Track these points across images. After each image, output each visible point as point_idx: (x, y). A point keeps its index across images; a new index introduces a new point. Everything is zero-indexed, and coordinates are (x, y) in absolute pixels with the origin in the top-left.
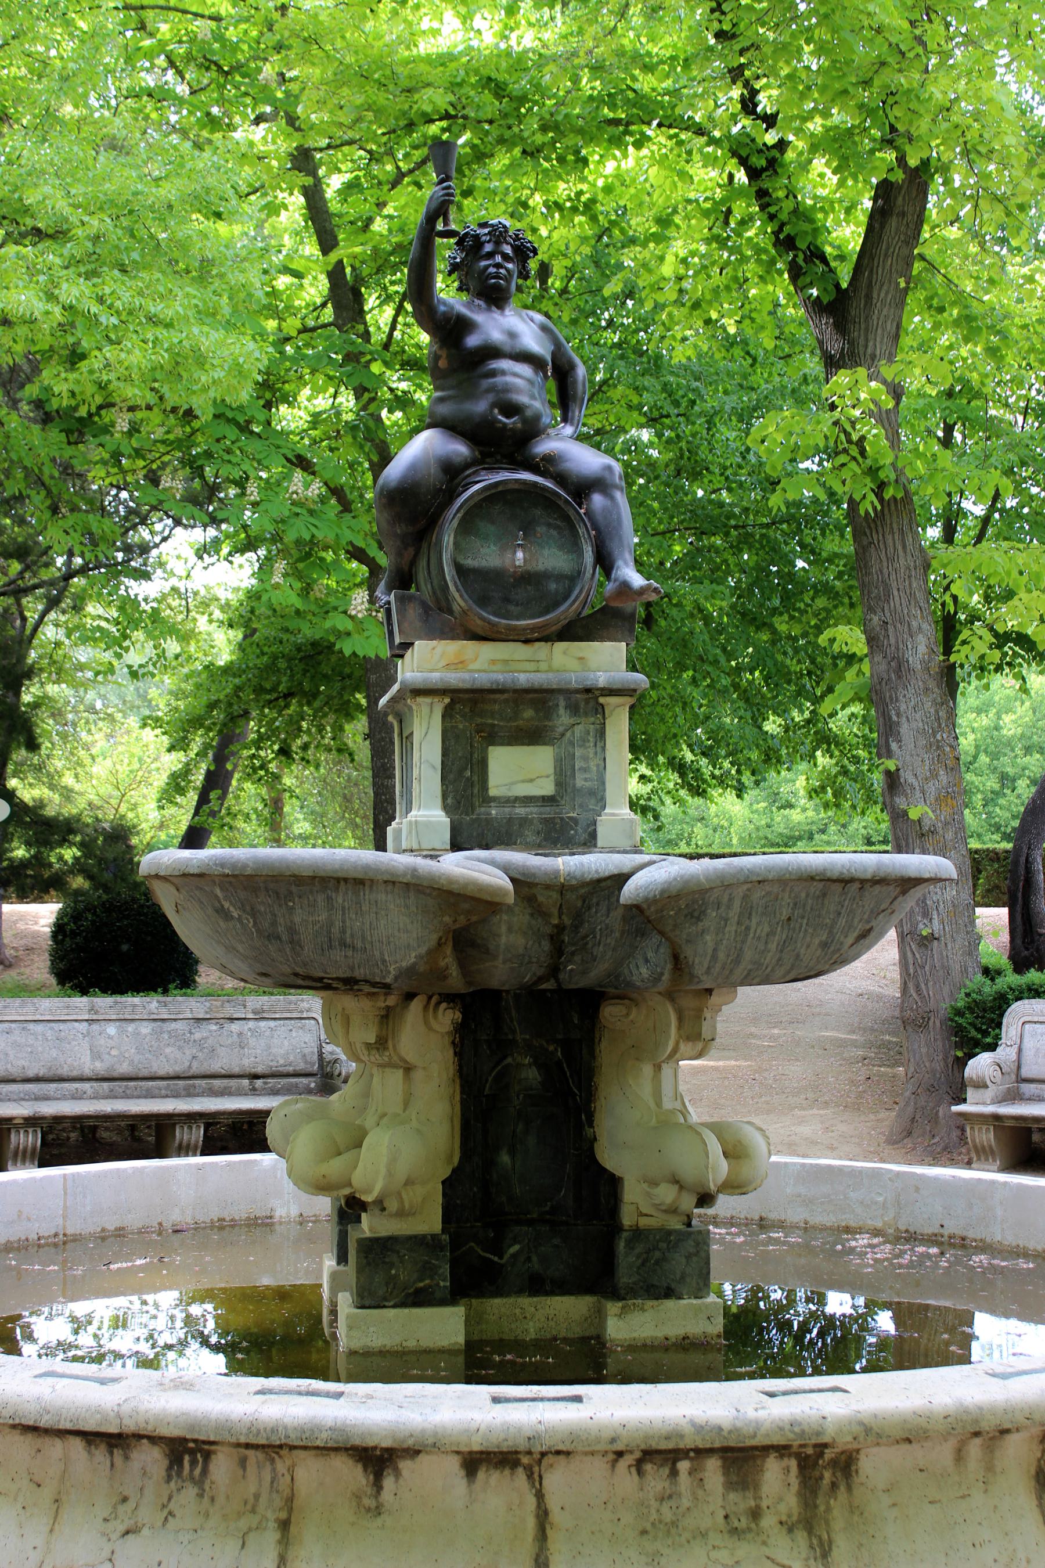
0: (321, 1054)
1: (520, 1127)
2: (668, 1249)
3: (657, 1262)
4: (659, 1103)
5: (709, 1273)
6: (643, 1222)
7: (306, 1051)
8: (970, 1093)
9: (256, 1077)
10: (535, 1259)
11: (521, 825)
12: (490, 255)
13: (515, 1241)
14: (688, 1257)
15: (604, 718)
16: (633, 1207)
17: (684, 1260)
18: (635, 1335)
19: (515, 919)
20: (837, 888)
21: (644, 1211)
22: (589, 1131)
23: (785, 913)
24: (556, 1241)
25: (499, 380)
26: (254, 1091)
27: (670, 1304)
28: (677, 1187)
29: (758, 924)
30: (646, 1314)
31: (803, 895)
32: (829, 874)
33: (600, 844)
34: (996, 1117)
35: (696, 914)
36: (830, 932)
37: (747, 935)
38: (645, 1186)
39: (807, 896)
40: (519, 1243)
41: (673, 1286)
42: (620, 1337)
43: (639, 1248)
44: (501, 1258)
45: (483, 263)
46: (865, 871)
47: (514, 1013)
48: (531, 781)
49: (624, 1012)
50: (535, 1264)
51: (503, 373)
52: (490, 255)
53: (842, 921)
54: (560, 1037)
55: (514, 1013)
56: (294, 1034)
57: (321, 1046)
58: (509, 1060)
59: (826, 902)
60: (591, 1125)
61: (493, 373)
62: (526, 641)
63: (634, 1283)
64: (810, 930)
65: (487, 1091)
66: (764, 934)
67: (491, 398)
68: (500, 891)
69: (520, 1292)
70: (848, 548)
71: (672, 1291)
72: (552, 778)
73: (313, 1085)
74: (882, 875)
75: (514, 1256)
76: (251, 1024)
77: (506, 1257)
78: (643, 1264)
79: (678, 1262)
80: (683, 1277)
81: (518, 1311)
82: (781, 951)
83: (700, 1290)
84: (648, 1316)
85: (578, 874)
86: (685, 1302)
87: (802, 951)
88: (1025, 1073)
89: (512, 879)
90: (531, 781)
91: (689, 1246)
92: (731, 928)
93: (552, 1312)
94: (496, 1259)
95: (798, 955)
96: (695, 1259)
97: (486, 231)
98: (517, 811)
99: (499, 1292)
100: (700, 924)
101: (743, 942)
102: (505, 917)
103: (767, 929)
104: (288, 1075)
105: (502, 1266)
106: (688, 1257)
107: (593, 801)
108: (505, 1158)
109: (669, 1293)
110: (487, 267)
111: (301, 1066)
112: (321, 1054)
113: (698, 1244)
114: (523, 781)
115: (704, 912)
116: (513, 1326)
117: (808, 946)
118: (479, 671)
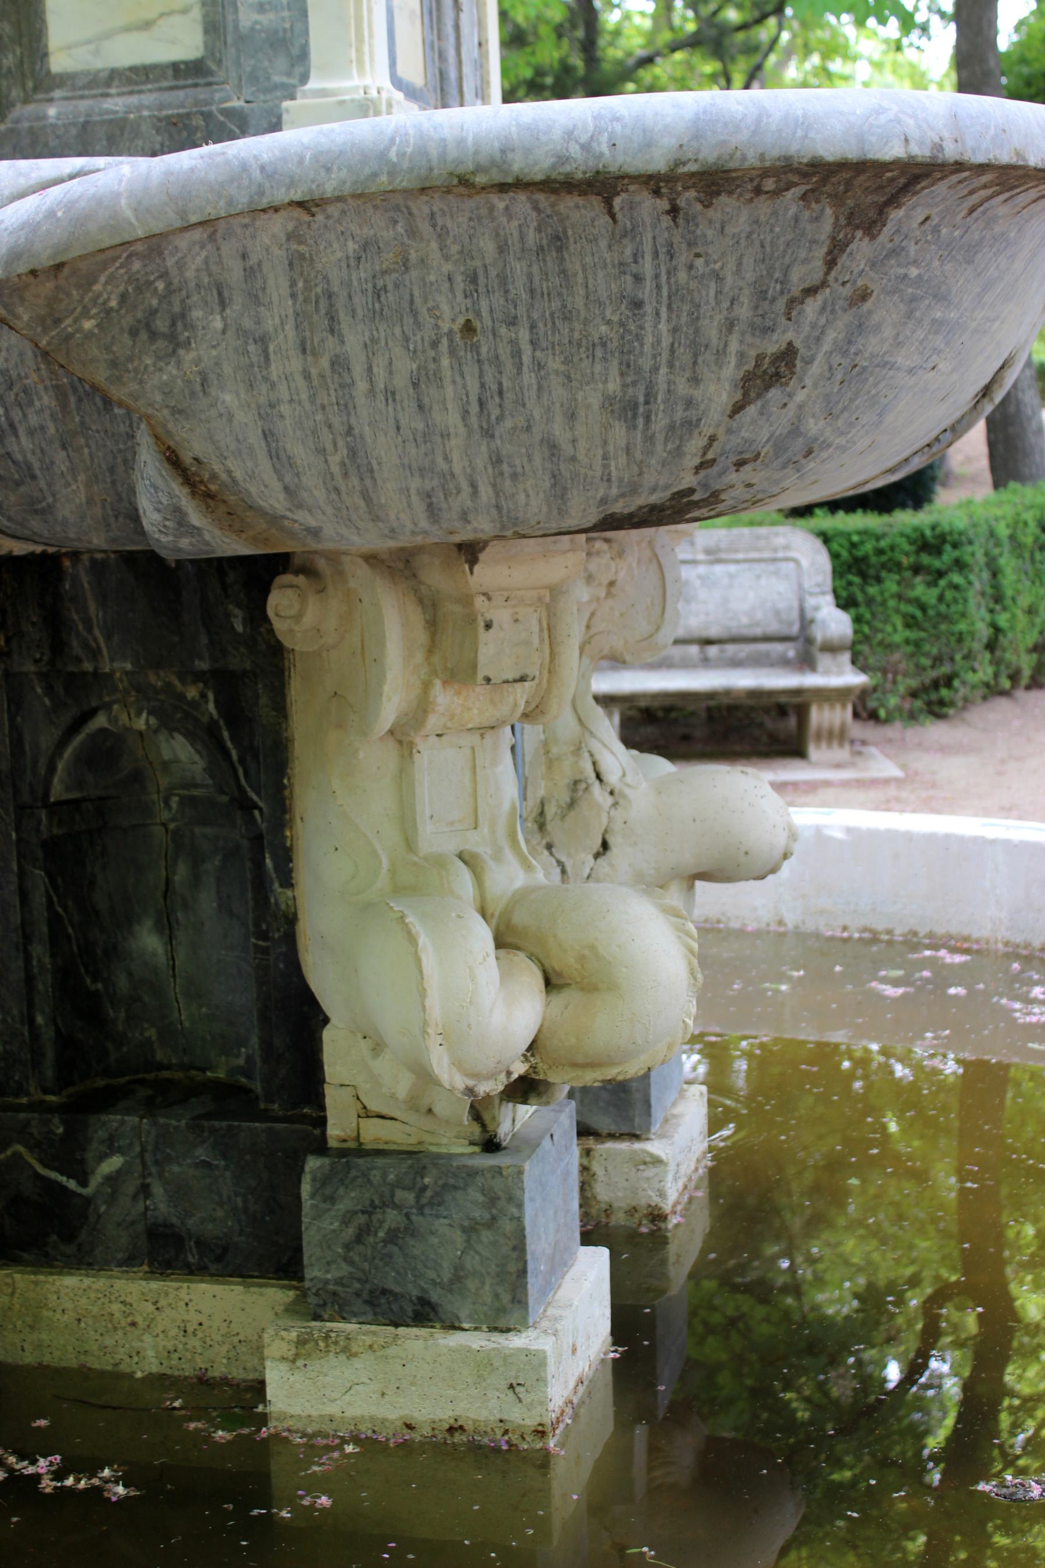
1: (182, 872)
2: (421, 1209)
3: (393, 1237)
5: (523, 1272)
6: (373, 1132)
7: (782, 605)
9: (708, 642)
10: (158, 1190)
13: (112, 1147)
14: (471, 1230)
16: (346, 1094)
17: (459, 1237)
18: (333, 1409)
20: (582, 213)
21: (374, 1107)
22: (280, 894)
23: (450, 312)
24: (201, 1153)
26: (706, 662)
27: (414, 1340)
29: (370, 346)
30: (357, 1363)
31: (488, 246)
32: (518, 165)
35: (161, 324)
36: (626, 368)
37: (347, 386)
39: (502, 249)
40: (120, 1150)
41: (434, 1296)
42: (296, 1410)
43: (349, 1200)
44: (84, 1183)
46: (649, 144)
47: (92, 607)
48: (147, 25)
50: (160, 1204)
53: (657, 331)
54: (203, 665)
55: (92, 607)
56: (763, 581)
58: (100, 721)
59: (574, 265)
60: (288, 882)
63: (339, 1282)
64: (554, 364)
65: (58, 791)
66: (401, 381)
69: (130, 1261)
71: (433, 1307)
72: (196, 13)
73: (791, 654)
74: (709, 155)
75: (113, 1180)
76: (702, 569)
77: (95, 1181)
78: (359, 1239)
79: (442, 1241)
80: (458, 1276)
81: (116, 1307)
82: (488, 433)
83: (501, 1311)
84: (361, 1367)
86: (456, 1339)
87: (559, 430)
90: (147, 25)
91: (470, 1203)
92: (286, 363)
93: (194, 1318)
94: (72, 1184)
95: (552, 447)
96: (486, 1236)
98: (108, 104)
99: (83, 1259)
100: (188, 357)
101: (346, 407)
103: (405, 366)
104: (755, 640)
105: (88, 1201)
106: (471, 1230)
107: (281, 62)
108: (148, 941)
109: (424, 1313)
111: (773, 627)
113: (493, 1200)
114: (128, 29)
115: (182, 317)
116: (109, 1341)
117: (571, 416)
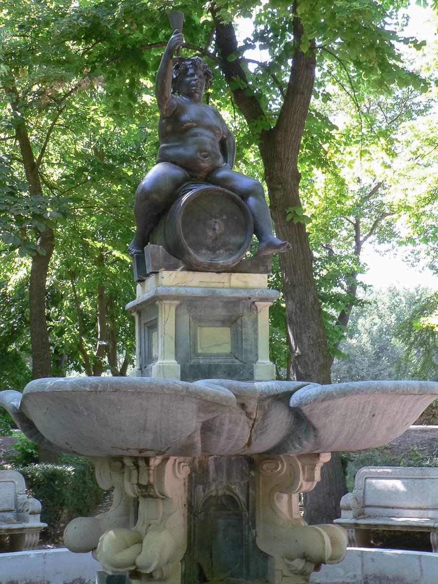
0: (16, 500)
4: (291, 516)
8: (343, 513)
11: (215, 368)
12: (193, 75)
15: (257, 313)
19: (233, 415)
25: (199, 138)
28: (304, 561)
33: (256, 378)
34: (356, 525)
38: (286, 560)
45: (188, 79)
49: (275, 466)
51: (201, 134)
52: (193, 75)
57: (17, 496)
61: (196, 135)
62: (218, 272)
67: (196, 147)
68: (231, 398)
70: (354, 233)
72: (230, 344)
85: (267, 391)
88: (367, 503)
89: (234, 394)
97: (190, 62)
102: (228, 415)
110: (190, 81)
112: (16, 500)
118: (195, 287)
